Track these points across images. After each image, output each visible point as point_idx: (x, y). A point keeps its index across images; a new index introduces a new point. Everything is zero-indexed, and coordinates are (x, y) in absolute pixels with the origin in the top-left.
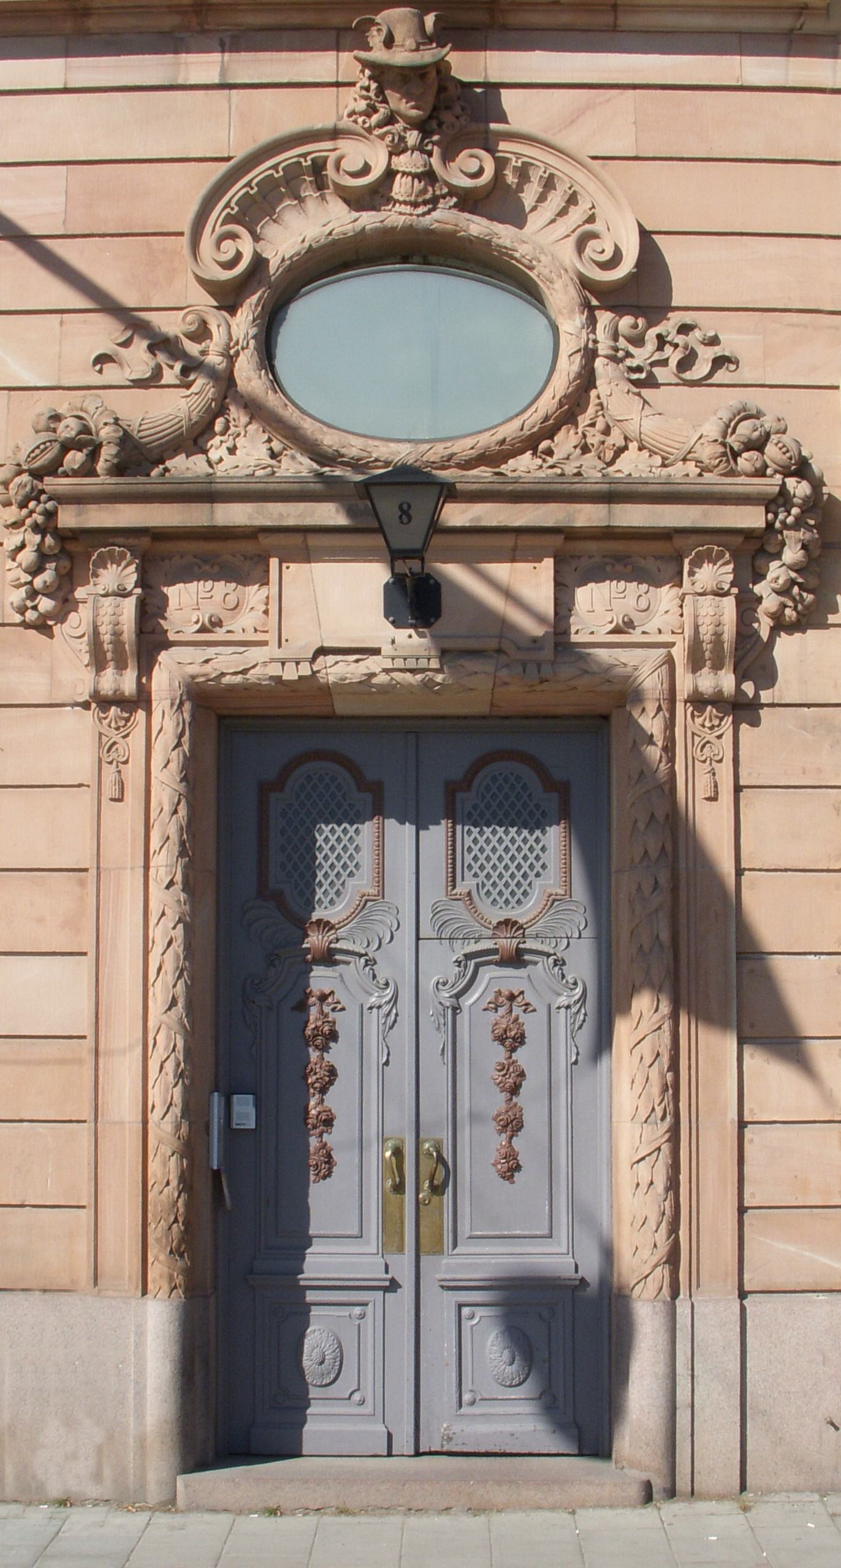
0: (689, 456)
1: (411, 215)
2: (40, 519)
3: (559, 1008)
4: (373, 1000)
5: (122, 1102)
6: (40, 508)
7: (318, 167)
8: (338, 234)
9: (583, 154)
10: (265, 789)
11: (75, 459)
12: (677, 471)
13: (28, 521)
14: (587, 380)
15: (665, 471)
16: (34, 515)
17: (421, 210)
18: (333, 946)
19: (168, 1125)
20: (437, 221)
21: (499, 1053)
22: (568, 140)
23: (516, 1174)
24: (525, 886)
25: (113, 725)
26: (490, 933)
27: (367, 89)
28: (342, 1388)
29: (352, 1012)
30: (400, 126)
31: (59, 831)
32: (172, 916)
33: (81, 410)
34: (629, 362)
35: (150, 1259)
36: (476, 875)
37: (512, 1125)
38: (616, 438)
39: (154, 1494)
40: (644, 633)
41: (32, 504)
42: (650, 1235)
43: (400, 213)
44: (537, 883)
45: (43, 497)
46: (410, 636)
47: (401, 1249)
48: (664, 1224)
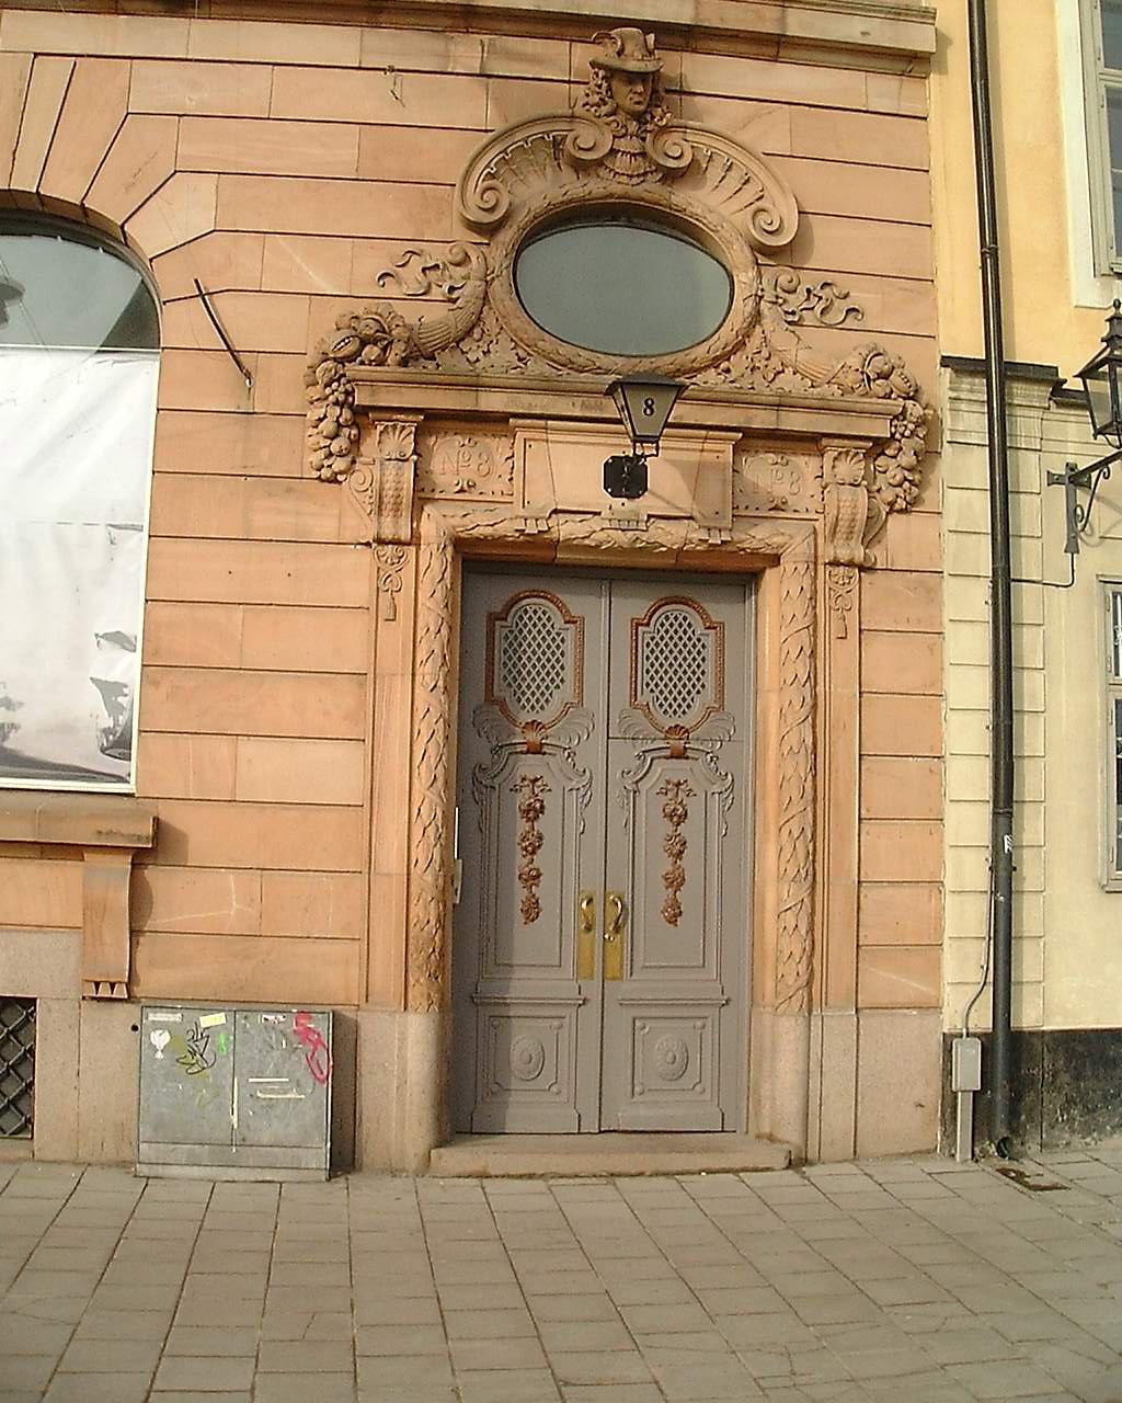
0: (833, 381)
1: (627, 184)
2: (341, 398)
3: (713, 793)
4: (574, 784)
5: (391, 858)
6: (342, 389)
7: (557, 144)
8: (571, 195)
9: (759, 150)
10: (493, 618)
11: (372, 352)
12: (824, 390)
13: (331, 398)
14: (757, 317)
15: (815, 391)
16: (336, 393)
17: (635, 180)
18: (543, 741)
19: (429, 878)
20: (646, 191)
21: (668, 827)
22: (743, 137)
23: (679, 919)
24: (689, 700)
25: (389, 561)
26: (663, 736)
27: (600, 86)
28: (543, 1083)
29: (557, 792)
30: (620, 117)
31: (346, 643)
32: (434, 714)
33: (376, 314)
34: (785, 307)
35: (412, 980)
36: (652, 691)
37: (676, 882)
38: (775, 363)
39: (412, 1163)
40: (795, 511)
41: (335, 385)
42: (794, 967)
43: (619, 183)
44: (698, 699)
45: (343, 380)
46: (623, 504)
47: (591, 977)
48: (804, 958)
